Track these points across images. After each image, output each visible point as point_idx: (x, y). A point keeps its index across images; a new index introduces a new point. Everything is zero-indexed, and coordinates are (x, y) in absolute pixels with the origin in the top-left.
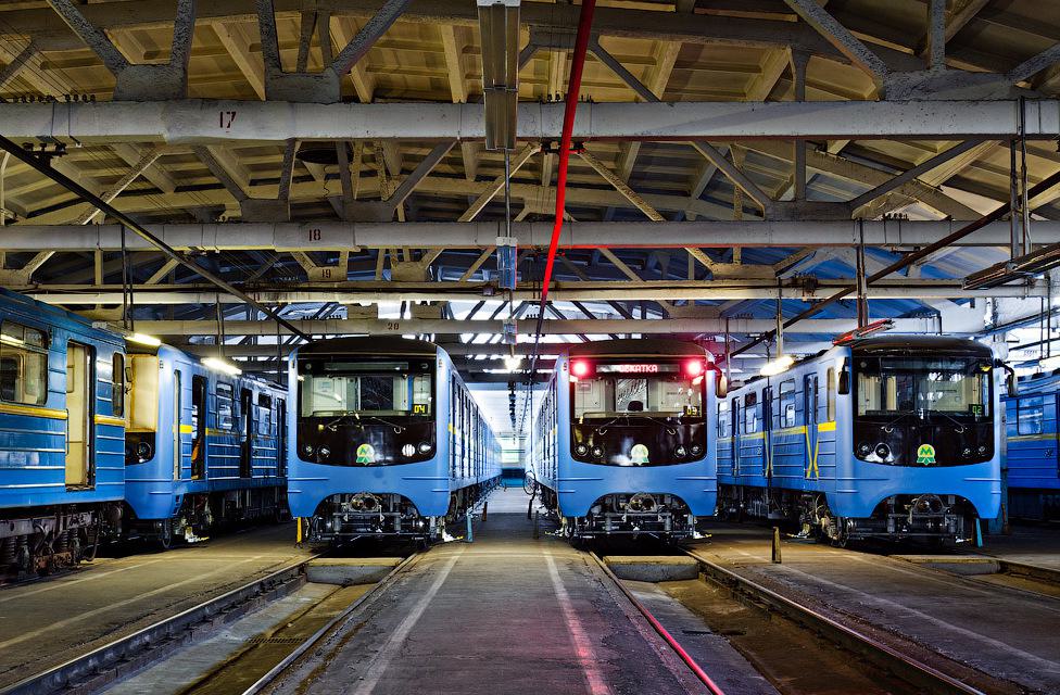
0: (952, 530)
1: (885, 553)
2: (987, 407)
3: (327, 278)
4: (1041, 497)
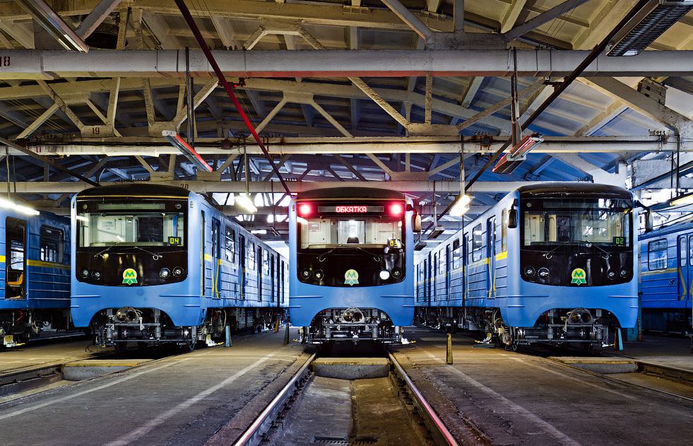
0: (599, 337)
1: (545, 355)
2: (628, 241)
3: (96, 133)
4: (665, 315)
